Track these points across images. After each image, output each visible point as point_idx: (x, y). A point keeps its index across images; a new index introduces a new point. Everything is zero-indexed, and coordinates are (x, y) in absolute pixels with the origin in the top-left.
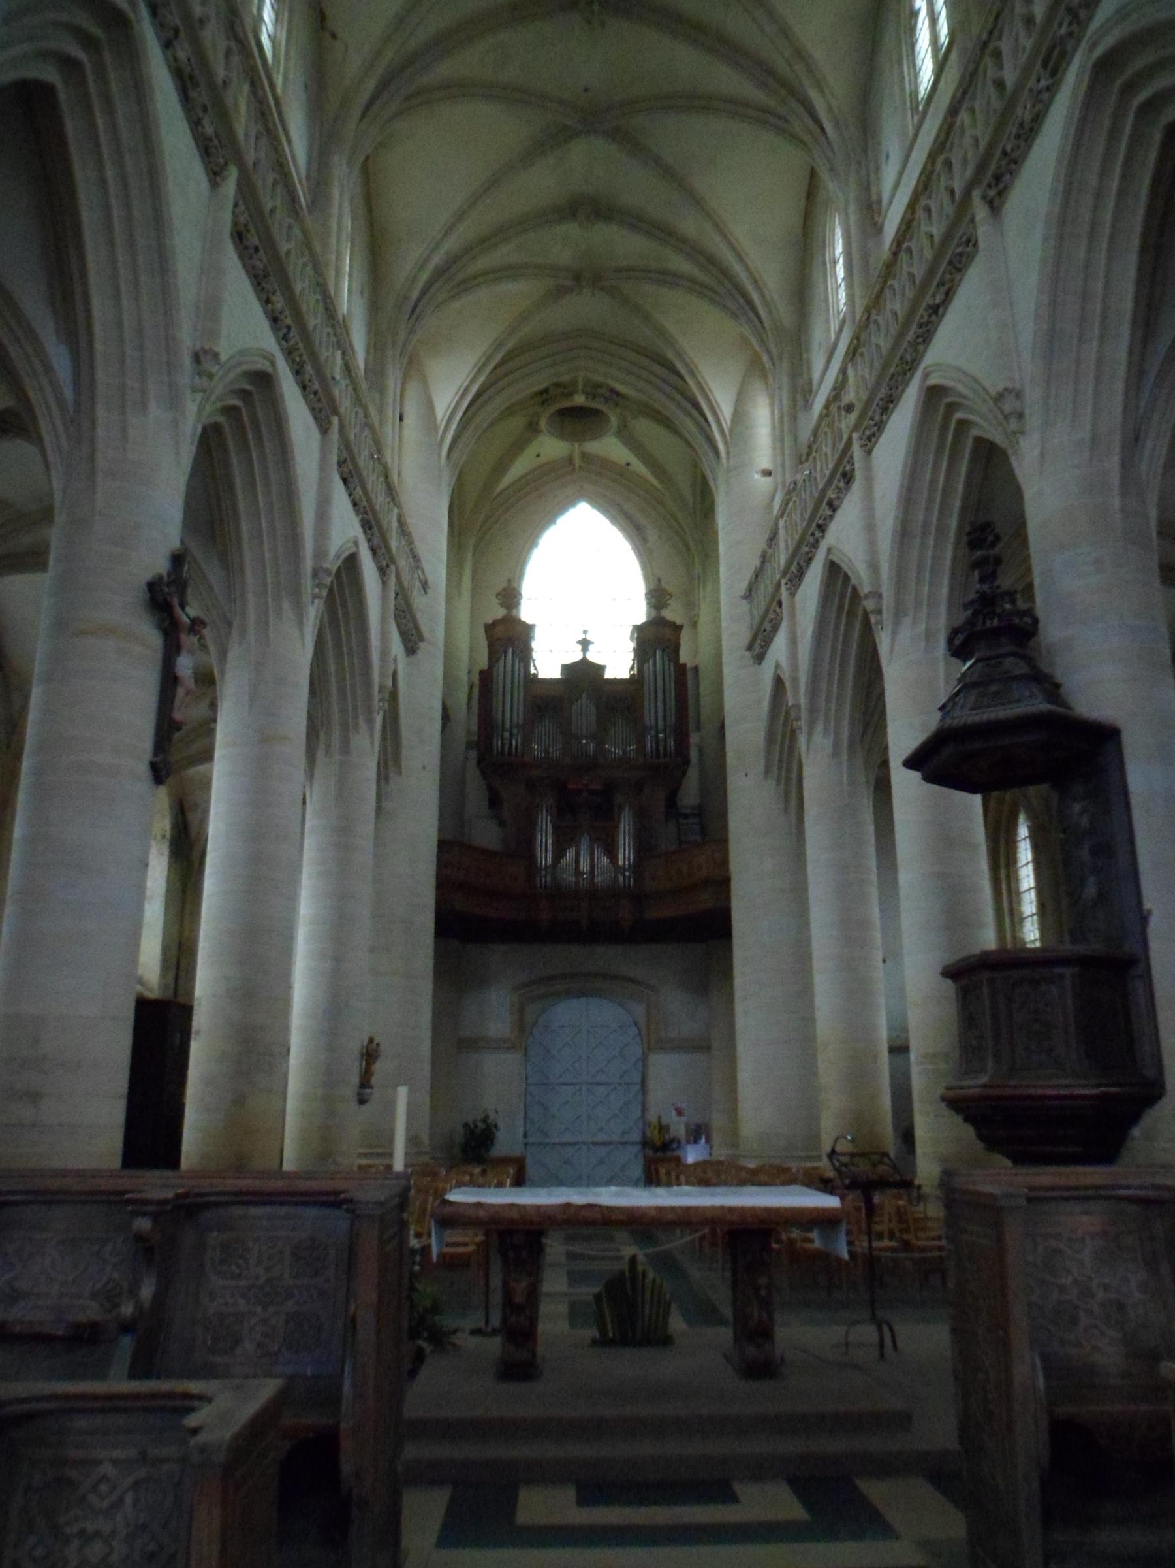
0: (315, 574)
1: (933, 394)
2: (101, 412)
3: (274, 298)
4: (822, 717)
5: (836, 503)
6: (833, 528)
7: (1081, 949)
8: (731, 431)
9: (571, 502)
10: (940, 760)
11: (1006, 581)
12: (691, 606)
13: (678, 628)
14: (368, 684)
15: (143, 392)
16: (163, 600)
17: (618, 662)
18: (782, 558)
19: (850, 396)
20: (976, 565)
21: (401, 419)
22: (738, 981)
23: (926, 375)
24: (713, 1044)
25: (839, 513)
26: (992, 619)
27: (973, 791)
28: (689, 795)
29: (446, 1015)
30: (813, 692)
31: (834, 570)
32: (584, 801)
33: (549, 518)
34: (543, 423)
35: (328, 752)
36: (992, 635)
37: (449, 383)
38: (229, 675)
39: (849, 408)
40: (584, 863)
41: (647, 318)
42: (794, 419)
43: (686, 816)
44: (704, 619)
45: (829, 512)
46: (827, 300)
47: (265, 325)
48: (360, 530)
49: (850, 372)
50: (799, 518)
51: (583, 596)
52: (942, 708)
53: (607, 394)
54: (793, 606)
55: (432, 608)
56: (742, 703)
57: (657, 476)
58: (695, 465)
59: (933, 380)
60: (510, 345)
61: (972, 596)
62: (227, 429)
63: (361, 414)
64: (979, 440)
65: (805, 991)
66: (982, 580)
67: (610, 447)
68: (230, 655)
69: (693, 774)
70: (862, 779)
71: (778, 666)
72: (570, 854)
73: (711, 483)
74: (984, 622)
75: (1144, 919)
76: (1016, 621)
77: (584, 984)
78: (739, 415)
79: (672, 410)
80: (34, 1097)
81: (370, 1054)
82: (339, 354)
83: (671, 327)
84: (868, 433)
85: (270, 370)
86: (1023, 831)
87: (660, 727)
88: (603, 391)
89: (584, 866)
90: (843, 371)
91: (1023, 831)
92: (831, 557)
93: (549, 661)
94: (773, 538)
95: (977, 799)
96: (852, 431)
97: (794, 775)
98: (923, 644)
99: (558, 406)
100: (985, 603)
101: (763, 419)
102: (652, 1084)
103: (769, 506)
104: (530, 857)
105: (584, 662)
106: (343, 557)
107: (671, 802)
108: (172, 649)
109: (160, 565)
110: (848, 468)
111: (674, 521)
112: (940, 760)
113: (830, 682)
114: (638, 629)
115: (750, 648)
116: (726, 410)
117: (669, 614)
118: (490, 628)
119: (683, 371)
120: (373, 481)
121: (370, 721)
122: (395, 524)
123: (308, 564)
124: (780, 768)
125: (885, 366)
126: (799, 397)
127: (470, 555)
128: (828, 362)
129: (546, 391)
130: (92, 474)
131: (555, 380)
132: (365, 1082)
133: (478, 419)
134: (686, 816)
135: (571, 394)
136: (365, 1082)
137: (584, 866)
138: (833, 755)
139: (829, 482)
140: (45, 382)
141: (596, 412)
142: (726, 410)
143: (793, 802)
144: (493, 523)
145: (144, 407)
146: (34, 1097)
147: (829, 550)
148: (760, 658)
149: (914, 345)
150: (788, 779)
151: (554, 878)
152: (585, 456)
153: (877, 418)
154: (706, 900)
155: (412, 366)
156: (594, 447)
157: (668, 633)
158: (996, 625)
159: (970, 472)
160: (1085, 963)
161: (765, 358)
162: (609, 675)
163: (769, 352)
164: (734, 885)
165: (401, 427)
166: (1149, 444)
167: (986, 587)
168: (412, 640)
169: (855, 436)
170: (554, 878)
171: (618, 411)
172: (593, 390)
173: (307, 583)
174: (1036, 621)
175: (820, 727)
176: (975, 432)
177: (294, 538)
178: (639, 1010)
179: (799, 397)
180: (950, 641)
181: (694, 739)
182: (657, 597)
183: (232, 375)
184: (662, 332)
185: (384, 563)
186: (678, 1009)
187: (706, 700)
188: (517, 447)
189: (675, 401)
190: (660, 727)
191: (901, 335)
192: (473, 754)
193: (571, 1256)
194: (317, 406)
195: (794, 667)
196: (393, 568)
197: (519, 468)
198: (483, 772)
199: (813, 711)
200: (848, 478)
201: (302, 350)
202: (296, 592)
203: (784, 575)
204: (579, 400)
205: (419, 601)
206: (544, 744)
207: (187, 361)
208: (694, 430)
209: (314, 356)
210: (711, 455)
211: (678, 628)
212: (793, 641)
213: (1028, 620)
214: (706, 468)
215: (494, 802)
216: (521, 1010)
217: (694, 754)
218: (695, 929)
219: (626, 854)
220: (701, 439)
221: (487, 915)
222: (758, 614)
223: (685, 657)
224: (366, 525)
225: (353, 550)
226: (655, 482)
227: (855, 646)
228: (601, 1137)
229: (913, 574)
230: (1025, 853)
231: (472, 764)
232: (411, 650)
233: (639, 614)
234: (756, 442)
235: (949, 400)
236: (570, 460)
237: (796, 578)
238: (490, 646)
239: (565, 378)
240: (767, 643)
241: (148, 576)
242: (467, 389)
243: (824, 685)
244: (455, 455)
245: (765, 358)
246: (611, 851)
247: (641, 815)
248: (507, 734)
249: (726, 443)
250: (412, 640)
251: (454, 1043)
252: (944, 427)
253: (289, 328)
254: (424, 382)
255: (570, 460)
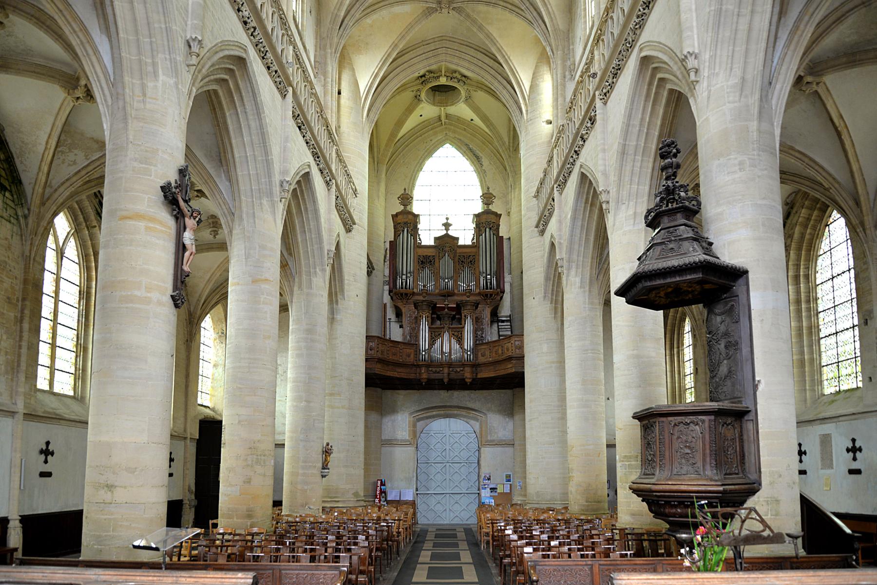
0: (281, 184)
1: (645, 61)
2: (127, 79)
3: (243, 9)
4: (574, 265)
5: (585, 137)
6: (584, 153)
7: (714, 405)
8: (529, 96)
9: (440, 144)
10: (638, 291)
11: (681, 179)
12: (507, 203)
13: (499, 216)
14: (321, 249)
15: (154, 64)
16: (175, 198)
17: (465, 234)
18: (555, 172)
19: (596, 68)
20: (663, 169)
21: (339, 93)
22: (527, 410)
23: (641, 50)
24: (516, 444)
25: (586, 142)
26: (672, 203)
27: (656, 308)
28: (505, 311)
29: (372, 432)
30: (570, 250)
31: (583, 176)
32: (446, 314)
33: (429, 153)
34: (423, 96)
35: (300, 287)
36: (671, 213)
37: (366, 71)
38: (234, 244)
39: (594, 75)
40: (447, 347)
41: (481, 28)
42: (564, 86)
43: (503, 321)
44: (514, 210)
45: (581, 143)
46: (585, 9)
47: (239, 26)
48: (312, 158)
49: (596, 53)
50: (564, 147)
51: (447, 196)
52: (639, 259)
53: (459, 77)
54: (560, 201)
55: (360, 207)
56: (532, 259)
57: (488, 127)
58: (510, 120)
59: (643, 54)
60: (401, 46)
61: (662, 189)
62: (221, 93)
63: (308, 87)
64: (671, 91)
65: (563, 417)
66: (667, 179)
67: (461, 110)
68: (234, 232)
69: (507, 297)
70: (596, 301)
71: (552, 236)
72: (439, 342)
73: (518, 129)
74: (667, 206)
75: (755, 387)
76: (687, 203)
77: (446, 411)
78: (534, 86)
79: (496, 86)
80: (110, 487)
81: (327, 452)
82: (291, 48)
83: (495, 34)
84: (604, 91)
85: (244, 56)
86: (687, 327)
87: (488, 272)
88: (457, 75)
89: (446, 349)
90: (592, 52)
91: (687, 327)
92: (582, 170)
93: (428, 234)
94: (550, 161)
95: (661, 313)
96: (596, 90)
97: (560, 299)
98: (632, 221)
99: (431, 85)
100: (669, 194)
101: (547, 85)
102: (482, 463)
103: (550, 142)
104: (416, 346)
105: (447, 236)
106: (301, 174)
107: (494, 314)
108: (181, 229)
109: (172, 177)
110: (593, 114)
111: (495, 151)
112: (638, 291)
113: (580, 245)
114: (477, 216)
115: (537, 227)
116: (527, 85)
117: (493, 208)
118: (394, 217)
119: (501, 61)
120: (317, 127)
121: (324, 270)
122: (334, 155)
123: (277, 178)
124: (552, 294)
125: (616, 46)
126: (567, 73)
127: (383, 176)
128: (585, 49)
129: (424, 76)
130: (125, 119)
131: (428, 68)
132: (325, 466)
133: (384, 93)
134: (503, 321)
135: (438, 77)
136: (325, 466)
137: (446, 349)
138: (581, 287)
139: (582, 124)
140: (94, 59)
141: (453, 88)
142: (527, 85)
143: (559, 314)
144: (396, 155)
145: (155, 74)
146: (110, 487)
147: (581, 166)
148: (542, 233)
149: (634, 31)
150: (556, 301)
151: (429, 355)
152: (448, 116)
153: (610, 81)
154: (510, 368)
155: (344, 61)
156: (452, 110)
157: (493, 218)
158: (676, 207)
159: (665, 113)
160: (719, 413)
161: (548, 49)
162: (461, 243)
163: (550, 45)
164: (525, 358)
165: (339, 99)
166: (778, 86)
167: (670, 183)
168: (348, 224)
169: (597, 93)
170: (429, 355)
171: (466, 87)
172: (452, 74)
173: (277, 189)
174: (699, 204)
175: (573, 272)
176: (669, 86)
177: (268, 163)
178: (477, 425)
179: (567, 73)
180: (646, 217)
181: (507, 278)
182: (487, 198)
183: (216, 58)
184: (489, 36)
185: (328, 179)
186: (499, 425)
187: (514, 256)
188: (409, 110)
189: (499, 83)
190: (488, 272)
191: (625, 26)
192: (387, 288)
193: (434, 557)
194: (278, 80)
195: (560, 237)
196: (334, 181)
197: (411, 123)
198: (392, 298)
199: (569, 261)
200: (593, 120)
201: (265, 44)
202: (270, 194)
203: (556, 182)
204: (443, 81)
205: (352, 202)
206: (426, 283)
207: (181, 45)
208: (507, 96)
209: (273, 48)
210: (518, 112)
211: (499, 216)
212: (560, 222)
213: (694, 202)
214: (514, 120)
215: (399, 314)
216: (415, 426)
217: (507, 288)
218: (504, 382)
219: (468, 341)
220: (511, 101)
221: (390, 376)
222: (542, 206)
223: (503, 232)
224: (315, 155)
225: (307, 170)
226: (487, 131)
227: (595, 223)
228: (456, 490)
229: (627, 179)
230: (688, 339)
231: (386, 293)
232: (349, 230)
233: (478, 207)
234: (543, 104)
235: (654, 65)
236: (439, 118)
237: (562, 184)
238: (395, 228)
239: (434, 67)
240: (546, 224)
241: (162, 182)
242: (377, 74)
243: (576, 247)
244: (372, 115)
245: (548, 49)
246: (460, 340)
247: (477, 321)
248: (404, 277)
249: (526, 105)
250: (348, 224)
251: (375, 444)
252: (650, 84)
253: (255, 28)
254: (353, 70)
255: (439, 118)
